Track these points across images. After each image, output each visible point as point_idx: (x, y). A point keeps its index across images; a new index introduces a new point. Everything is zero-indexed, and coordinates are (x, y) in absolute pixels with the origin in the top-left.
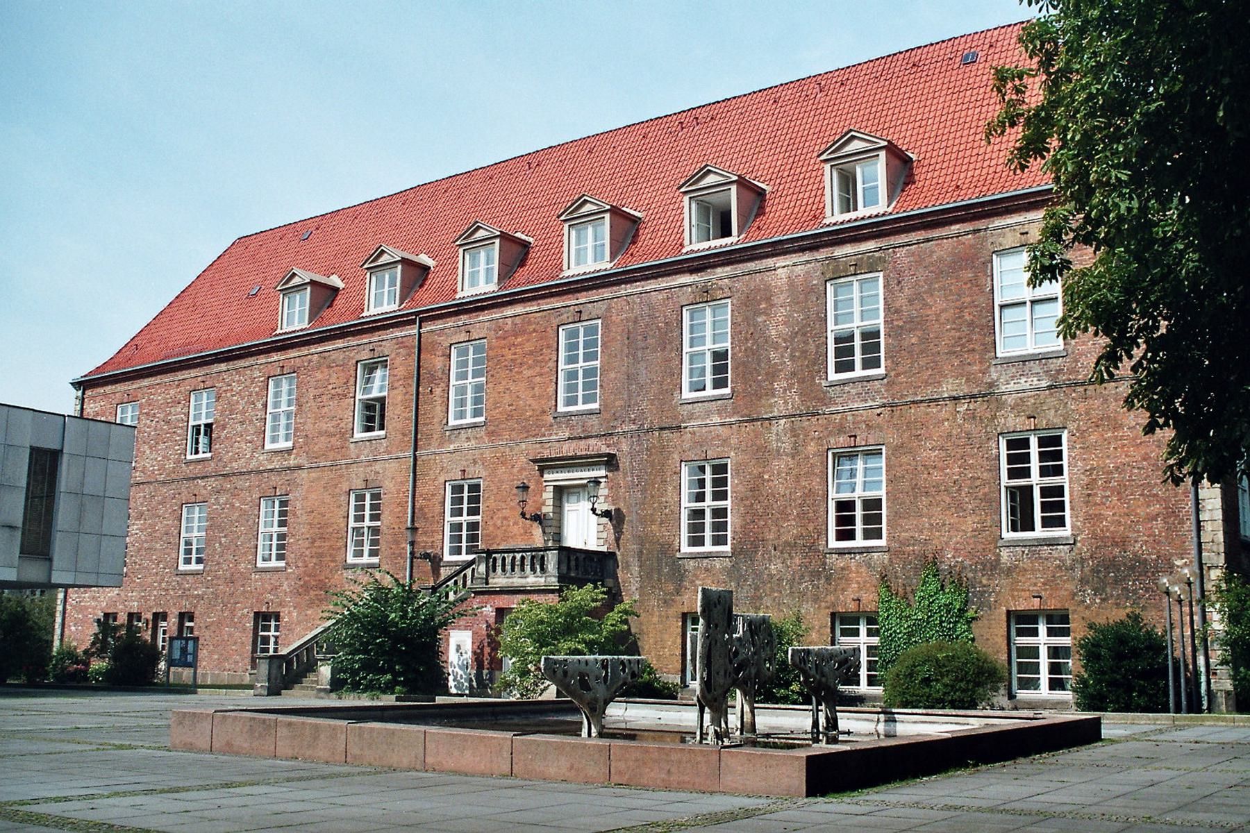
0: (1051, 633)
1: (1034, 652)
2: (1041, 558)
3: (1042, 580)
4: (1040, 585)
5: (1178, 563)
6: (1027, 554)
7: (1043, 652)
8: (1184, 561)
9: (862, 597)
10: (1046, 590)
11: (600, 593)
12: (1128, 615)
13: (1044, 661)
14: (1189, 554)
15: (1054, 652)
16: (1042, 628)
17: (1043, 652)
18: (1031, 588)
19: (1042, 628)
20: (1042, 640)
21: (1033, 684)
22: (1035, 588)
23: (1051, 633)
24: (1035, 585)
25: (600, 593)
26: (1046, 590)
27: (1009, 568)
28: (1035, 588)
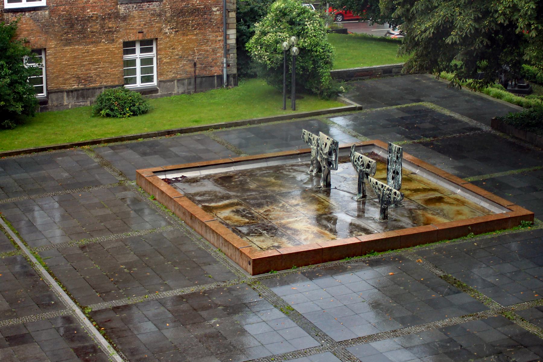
0: (142, 51)
1: (133, 62)
2: (143, 10)
3: (143, 23)
4: (142, 25)
5: (214, 9)
6: (135, 8)
7: (138, 62)
8: (217, 8)
9: (30, 40)
10: (146, 28)
11: (62, 334)
12: (475, 91)
13: (138, 67)
14: (219, 4)
15: (144, 61)
16: (138, 48)
17: (138, 62)
18: (137, 27)
19: (138, 48)
20: (138, 55)
21: (134, 81)
22: (140, 27)
23: (142, 51)
24: (139, 25)
25: (62, 334)
26: (146, 28)
27: (125, 17)
28: (140, 27)
